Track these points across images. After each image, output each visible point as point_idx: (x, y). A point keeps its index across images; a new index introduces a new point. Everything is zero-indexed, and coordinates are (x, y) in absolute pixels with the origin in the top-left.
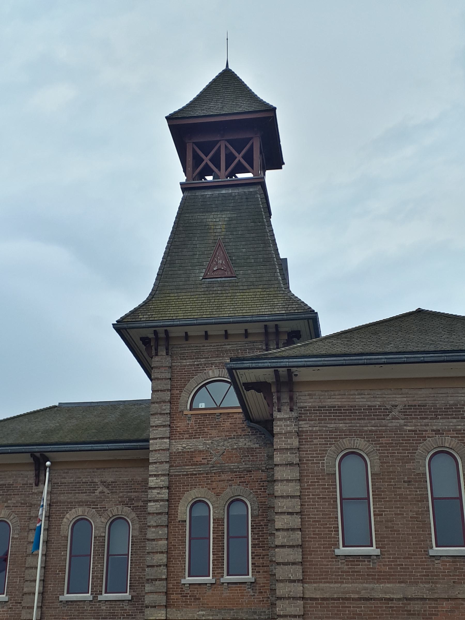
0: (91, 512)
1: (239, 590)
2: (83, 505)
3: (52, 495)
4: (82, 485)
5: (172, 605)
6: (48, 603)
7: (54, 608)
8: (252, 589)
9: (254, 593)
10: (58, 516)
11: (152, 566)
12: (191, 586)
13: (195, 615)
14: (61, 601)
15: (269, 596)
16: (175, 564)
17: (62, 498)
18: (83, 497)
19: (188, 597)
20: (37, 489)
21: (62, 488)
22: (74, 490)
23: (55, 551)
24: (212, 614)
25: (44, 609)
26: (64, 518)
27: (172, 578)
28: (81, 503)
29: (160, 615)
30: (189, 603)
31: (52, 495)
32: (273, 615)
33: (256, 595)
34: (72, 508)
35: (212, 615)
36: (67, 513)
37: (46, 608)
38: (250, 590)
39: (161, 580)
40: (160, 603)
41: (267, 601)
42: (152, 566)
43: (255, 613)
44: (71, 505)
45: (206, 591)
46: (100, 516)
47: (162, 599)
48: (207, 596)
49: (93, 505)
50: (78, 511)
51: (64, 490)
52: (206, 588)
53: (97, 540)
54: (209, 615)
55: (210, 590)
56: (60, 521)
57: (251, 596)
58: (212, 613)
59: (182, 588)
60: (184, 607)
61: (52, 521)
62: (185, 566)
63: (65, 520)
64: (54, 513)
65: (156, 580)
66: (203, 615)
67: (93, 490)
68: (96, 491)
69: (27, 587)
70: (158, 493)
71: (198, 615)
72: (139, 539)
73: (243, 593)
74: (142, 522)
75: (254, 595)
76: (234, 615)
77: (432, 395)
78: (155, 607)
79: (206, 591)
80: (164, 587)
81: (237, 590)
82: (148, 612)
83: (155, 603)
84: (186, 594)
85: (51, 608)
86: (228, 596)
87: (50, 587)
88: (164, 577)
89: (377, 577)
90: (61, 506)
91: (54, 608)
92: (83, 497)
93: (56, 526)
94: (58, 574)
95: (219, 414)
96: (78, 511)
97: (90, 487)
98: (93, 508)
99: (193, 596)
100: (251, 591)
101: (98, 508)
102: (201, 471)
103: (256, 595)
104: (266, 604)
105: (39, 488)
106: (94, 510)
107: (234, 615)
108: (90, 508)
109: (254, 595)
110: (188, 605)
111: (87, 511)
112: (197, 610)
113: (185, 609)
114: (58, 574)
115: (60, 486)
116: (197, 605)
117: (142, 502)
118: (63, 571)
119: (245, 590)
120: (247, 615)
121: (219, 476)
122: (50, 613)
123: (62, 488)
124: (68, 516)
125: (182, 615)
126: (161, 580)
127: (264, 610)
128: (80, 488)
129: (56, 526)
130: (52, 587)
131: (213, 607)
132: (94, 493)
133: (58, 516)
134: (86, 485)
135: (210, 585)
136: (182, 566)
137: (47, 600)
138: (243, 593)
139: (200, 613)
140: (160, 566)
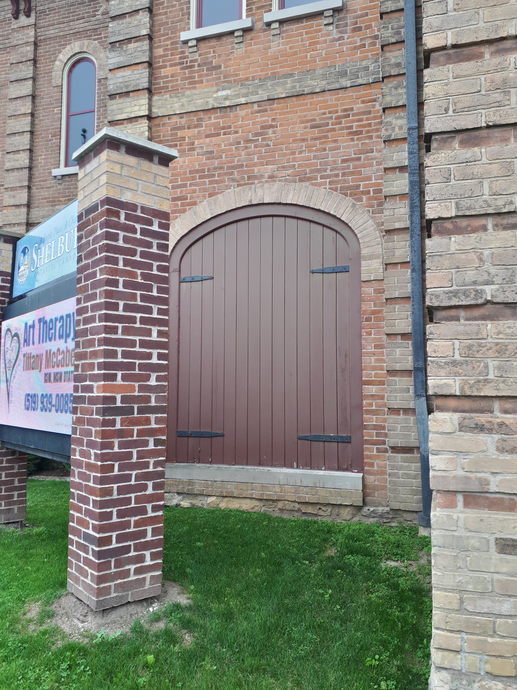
0: (93, 46)
1: (307, 33)
2: (81, 38)
3: (38, 30)
4: (77, 8)
5: (163, 88)
6: (40, 181)
7: (46, 188)
8: (337, 27)
9: (341, 32)
10: (47, 59)
11: (122, 16)
12: (202, 45)
14: (55, 177)
15: (377, 33)
16: (168, 7)
17: (52, 32)
18: (80, 25)
19: (196, 68)
20: (16, 23)
21: (51, 17)
22: (67, 17)
23: (47, 108)
25: (34, 190)
26: (55, 61)
27: (164, 35)
28: (78, 35)
30: (196, 79)
31: (38, 30)
32: (387, 68)
33: (346, 36)
34: (66, 44)
35: (246, 95)
36: (60, 53)
37: (37, 189)
38: (331, 28)
39: (137, 38)
40: (138, 85)
41: (374, 44)
42: (122, 16)
43: (343, 74)
44: (64, 40)
45: (233, 48)
46: (105, 48)
47: (140, 77)
48: (235, 59)
49: (95, 35)
50: (76, 46)
51: (53, 20)
52: (232, 43)
53: (102, 85)
54: (238, 96)
55: (242, 45)
56: (50, 65)
57: (334, 40)
58: (244, 91)
59: (183, 52)
60: (187, 88)
61: (40, 67)
62: (189, 8)
63: (57, 63)
64: (43, 56)
65: (129, 40)
66: (226, 98)
67: (93, 12)
68: (97, 13)
69: (10, 161)
71: (216, 99)
73: (315, 37)
75: (340, 39)
76: (294, 87)
77: (466, 109)
79: (233, 48)
80: (144, 51)
81: (301, 34)
82: (114, 107)
83: (127, 87)
84: (191, 61)
85: (42, 188)
86: (280, 51)
87: (41, 159)
88: (145, 32)
90: (50, 44)
91: (46, 188)
92: (80, 25)
93: (46, 73)
94: (50, 140)
96: (76, 46)
97: (89, 9)
98: (95, 40)
99: (205, 64)
100: (335, 31)
101: (101, 38)
103: (346, 36)
104: (369, 51)
105: (19, 22)
106: (96, 42)
107: (294, 87)
108: (91, 39)
109: (340, 39)
111: (86, 44)
112: (215, 89)
113: (188, 93)
114: (50, 140)
115: (48, 15)
116: (213, 79)
118: (58, 135)
119: (320, 31)
120: (324, 82)
122: (41, 196)
123: (51, 17)
124: (61, 56)
125: (183, 105)
126: (137, 38)
127: (364, 63)
128: (76, 12)
129: (46, 73)
130: (44, 159)
131: (247, 79)
132: (95, 16)
133: (47, 59)
134: (84, 7)
135: (240, 33)
136: (182, 9)
137: (38, 178)
138: (315, 37)
140: (137, 11)
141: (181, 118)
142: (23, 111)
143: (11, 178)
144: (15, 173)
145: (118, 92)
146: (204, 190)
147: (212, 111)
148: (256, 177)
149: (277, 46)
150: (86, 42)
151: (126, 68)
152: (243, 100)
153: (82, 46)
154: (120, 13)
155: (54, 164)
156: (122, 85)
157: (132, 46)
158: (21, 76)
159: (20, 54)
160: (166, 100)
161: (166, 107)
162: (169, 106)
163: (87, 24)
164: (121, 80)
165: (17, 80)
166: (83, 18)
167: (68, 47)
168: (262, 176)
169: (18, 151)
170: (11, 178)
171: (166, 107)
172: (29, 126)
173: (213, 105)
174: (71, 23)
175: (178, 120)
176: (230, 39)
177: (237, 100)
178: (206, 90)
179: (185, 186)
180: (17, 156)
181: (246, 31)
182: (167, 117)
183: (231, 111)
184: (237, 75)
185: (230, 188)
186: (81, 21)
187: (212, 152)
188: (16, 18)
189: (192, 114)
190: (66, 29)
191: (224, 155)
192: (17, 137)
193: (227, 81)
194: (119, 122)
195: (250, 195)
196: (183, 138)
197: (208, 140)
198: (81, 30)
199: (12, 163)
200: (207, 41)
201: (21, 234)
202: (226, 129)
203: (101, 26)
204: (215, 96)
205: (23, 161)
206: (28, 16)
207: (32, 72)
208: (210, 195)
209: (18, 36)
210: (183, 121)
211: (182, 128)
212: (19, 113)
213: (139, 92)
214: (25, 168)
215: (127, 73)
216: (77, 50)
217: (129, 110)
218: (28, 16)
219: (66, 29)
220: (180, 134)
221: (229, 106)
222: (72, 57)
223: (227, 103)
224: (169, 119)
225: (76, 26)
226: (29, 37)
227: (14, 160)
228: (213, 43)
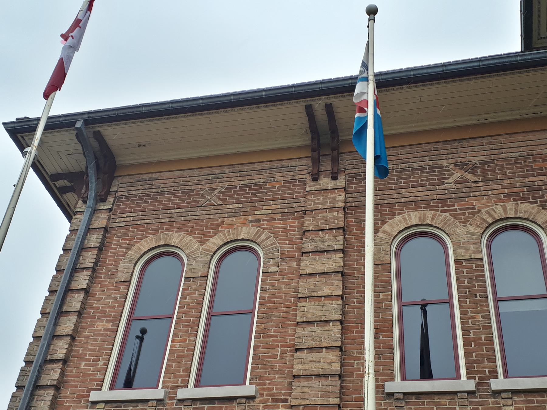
4: (413, 174)
18: (420, 193)
22: (397, 183)
28: (414, 204)
34: (395, 214)
49: (442, 206)
68: (446, 181)
92: (420, 193)
106: (447, 214)
142: (327, 291)
143: (306, 390)
144: (314, 382)
150: (429, 214)
153: (446, 222)
155: (385, 375)
158: (326, 245)
159: (319, 220)
163: (429, 193)
165: (316, 252)
166: (425, 185)
167: (398, 218)
169: (319, 349)
170: (306, 390)
172: (339, 313)
174: (403, 191)
180: (316, 356)
186: (420, 189)
188: (315, 179)
190: (395, 196)
191: (474, 268)
192: (315, 328)
198: (419, 199)
199: (308, 366)
201: (350, 78)
203: (454, 196)
205: (329, 364)
206: (335, 178)
207: (342, 242)
209: (318, 199)
212: (320, 293)
214: (333, 375)
216: (415, 221)
218: (335, 178)
219: (395, 196)
222: (405, 229)
225: (412, 194)
226: (337, 202)
227: (311, 361)
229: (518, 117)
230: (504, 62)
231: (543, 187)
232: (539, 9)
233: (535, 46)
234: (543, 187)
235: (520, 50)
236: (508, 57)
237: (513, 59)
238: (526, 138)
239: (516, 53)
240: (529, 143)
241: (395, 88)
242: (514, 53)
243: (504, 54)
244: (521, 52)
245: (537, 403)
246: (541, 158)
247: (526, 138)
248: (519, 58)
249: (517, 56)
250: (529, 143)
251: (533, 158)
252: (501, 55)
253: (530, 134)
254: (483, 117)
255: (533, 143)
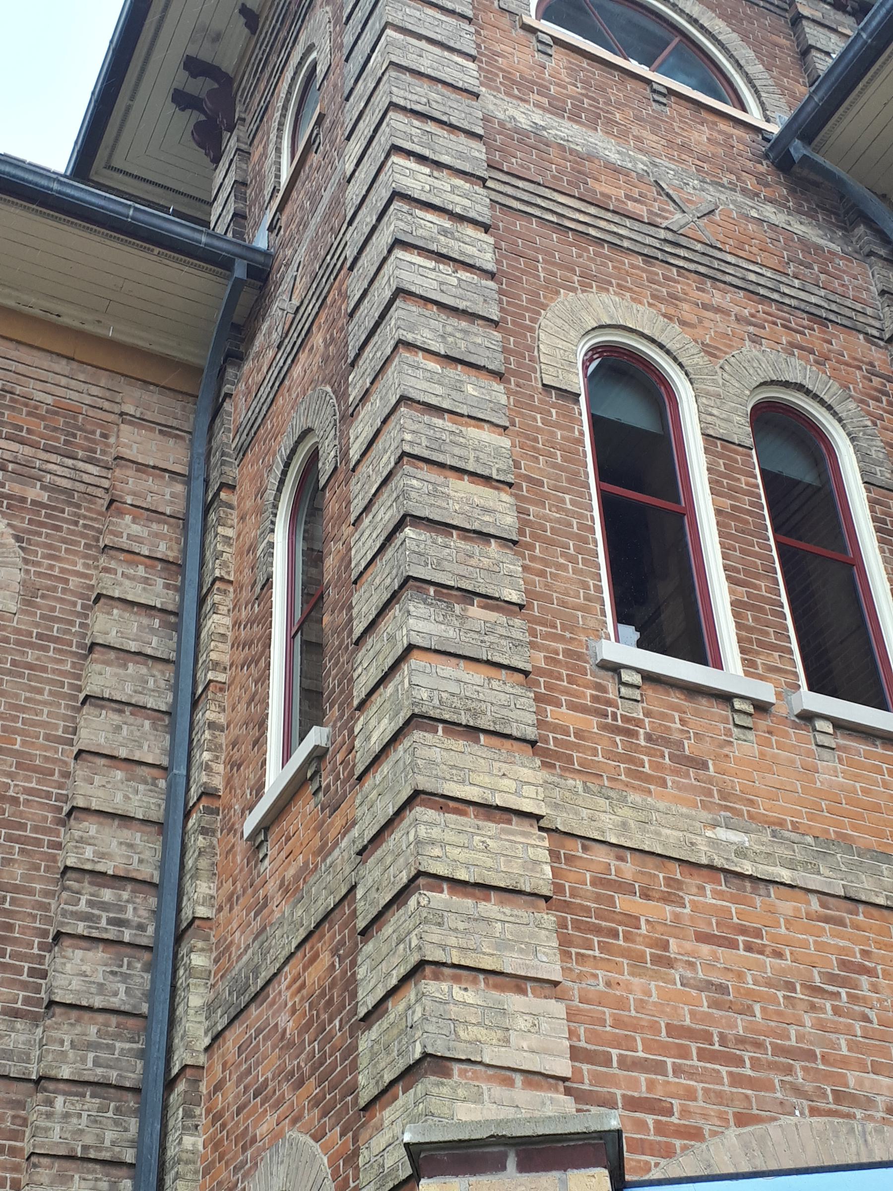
13: (698, 840)
24: (788, 853)
29: (506, 783)
35: (791, 865)
40: (505, 720)
45: (729, 733)
66: (741, 853)
70: (444, 232)
71: (714, 843)
72: (17, 631)
74: (35, 564)
78: (473, 732)
83: (475, 714)
89: (674, 1120)
95: (664, 91)
102: (621, 237)
110: (647, 778)
117: (43, 488)
121: (698, 289)
125: (624, 824)
136: (586, 587)
139: (722, 834)
141: (621, 859)
145: (446, 717)
146: (720, 1098)
147: (705, 871)
148: (853, 1100)
149: (831, 773)
151: (462, 663)
152: (786, 875)
154: (437, 518)
156: (457, 703)
157: (475, 611)
160: (573, 791)
161: (576, 813)
162: (585, 813)
164: (454, 688)
168: (869, 1103)
171: (576, 813)
173: (712, 860)
175: (614, 863)
176: (718, 710)
177: (770, 869)
178: (684, 810)
179: (659, 1068)
181: (762, 707)
182: (579, 842)
183: (754, 891)
184: (751, 803)
185: (793, 1114)
187: (722, 989)
189: (649, 860)
193: (729, 806)
194: (452, 804)
195: (854, 1149)
196: (633, 921)
197: (705, 949)
200: (660, 688)
202: (750, 937)
204: (709, 833)
205: (141, 861)
208: (742, 1120)
210: (629, 869)
211: (626, 888)
213: (508, 743)
215: (474, 676)
217: (485, 780)
220: (622, 903)
221: (750, 877)
223: (747, 868)
224: (585, 848)
228: (676, 698)
229: (11, 303)
230: (23, 180)
231: (11, 467)
232: (128, 109)
233: (95, 179)
234: (11, 467)
235: (62, 171)
236: (11, 164)
237: (44, 182)
238: (13, 354)
239: (54, 173)
240: (13, 366)
241: (157, 250)
242: (49, 171)
243: (30, 164)
244: (65, 176)
245: (732, 1085)
246: (26, 405)
247: (13, 354)
248: (55, 186)
249: (54, 180)
250: (13, 366)
251: (12, 400)
252: (24, 162)
253: (35, 353)
254: (47, 305)
255: (21, 368)
